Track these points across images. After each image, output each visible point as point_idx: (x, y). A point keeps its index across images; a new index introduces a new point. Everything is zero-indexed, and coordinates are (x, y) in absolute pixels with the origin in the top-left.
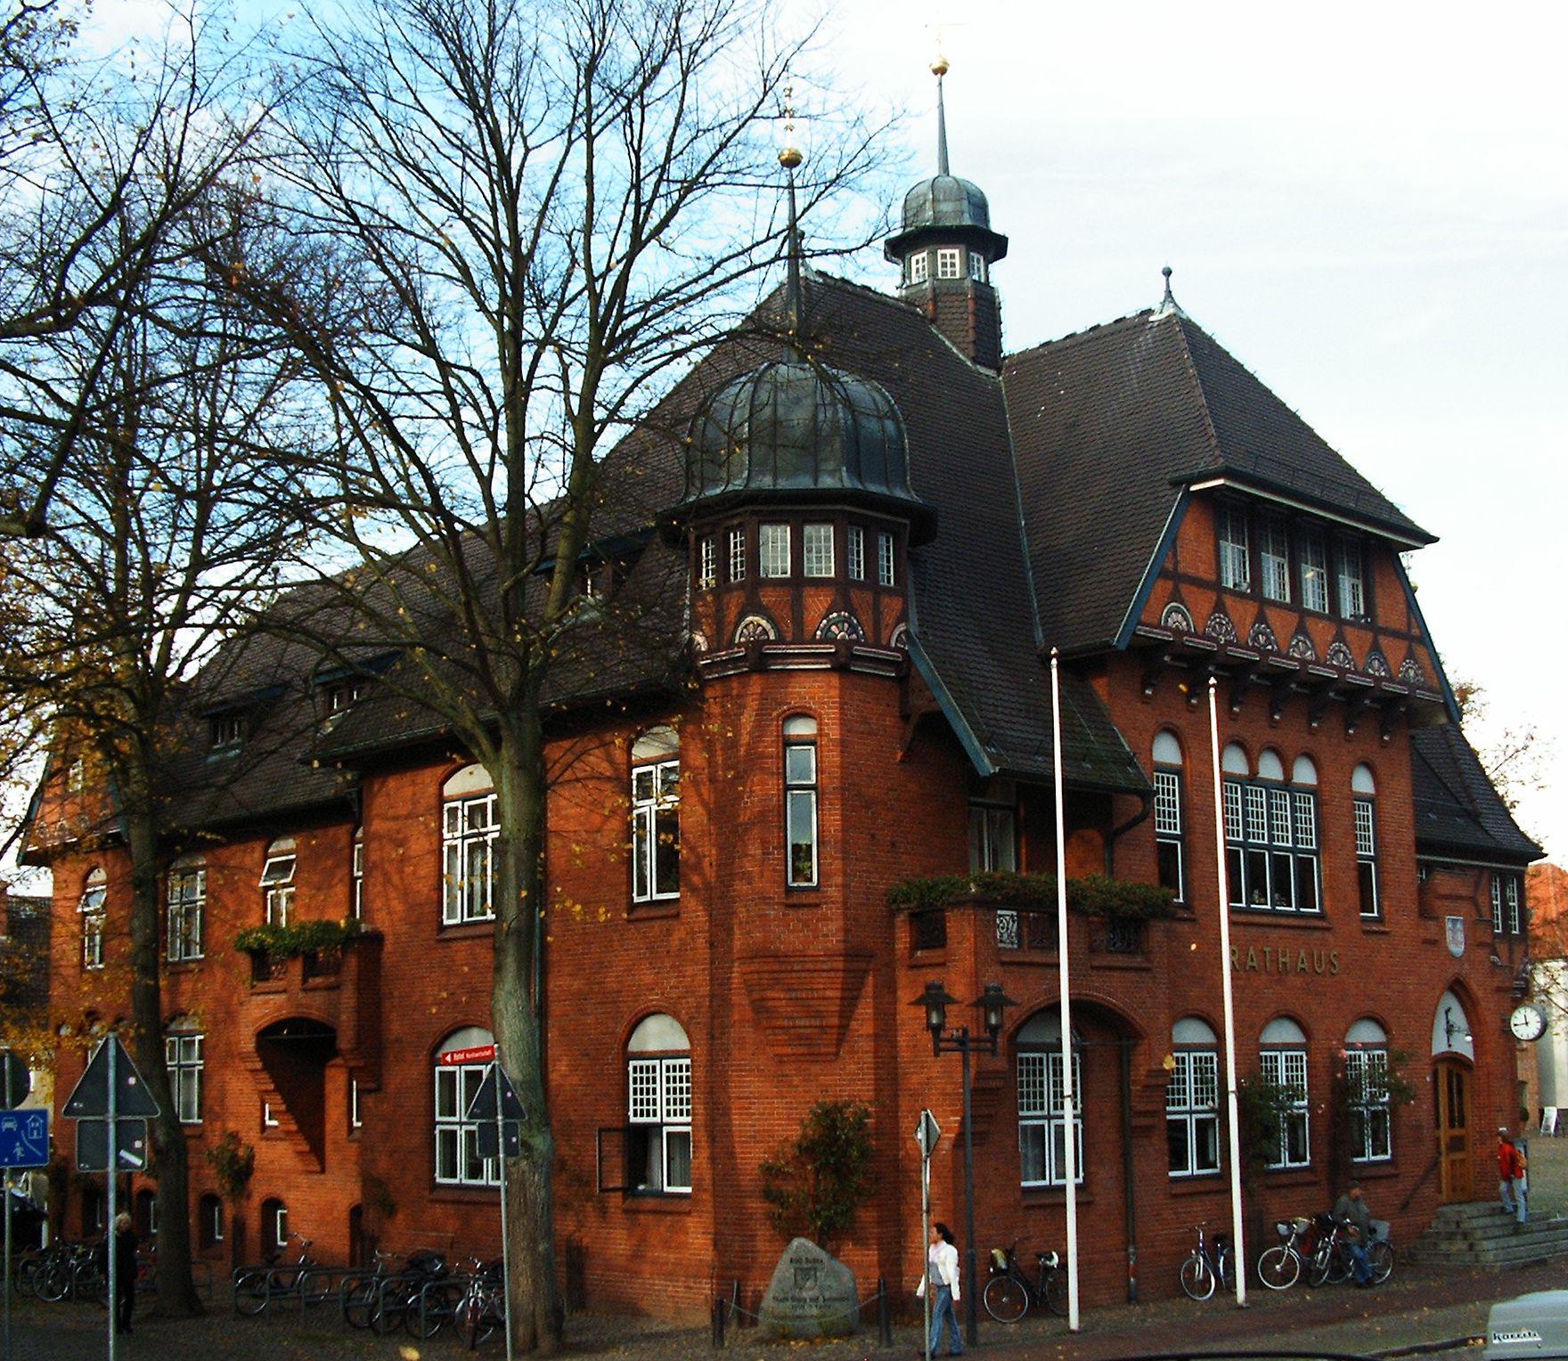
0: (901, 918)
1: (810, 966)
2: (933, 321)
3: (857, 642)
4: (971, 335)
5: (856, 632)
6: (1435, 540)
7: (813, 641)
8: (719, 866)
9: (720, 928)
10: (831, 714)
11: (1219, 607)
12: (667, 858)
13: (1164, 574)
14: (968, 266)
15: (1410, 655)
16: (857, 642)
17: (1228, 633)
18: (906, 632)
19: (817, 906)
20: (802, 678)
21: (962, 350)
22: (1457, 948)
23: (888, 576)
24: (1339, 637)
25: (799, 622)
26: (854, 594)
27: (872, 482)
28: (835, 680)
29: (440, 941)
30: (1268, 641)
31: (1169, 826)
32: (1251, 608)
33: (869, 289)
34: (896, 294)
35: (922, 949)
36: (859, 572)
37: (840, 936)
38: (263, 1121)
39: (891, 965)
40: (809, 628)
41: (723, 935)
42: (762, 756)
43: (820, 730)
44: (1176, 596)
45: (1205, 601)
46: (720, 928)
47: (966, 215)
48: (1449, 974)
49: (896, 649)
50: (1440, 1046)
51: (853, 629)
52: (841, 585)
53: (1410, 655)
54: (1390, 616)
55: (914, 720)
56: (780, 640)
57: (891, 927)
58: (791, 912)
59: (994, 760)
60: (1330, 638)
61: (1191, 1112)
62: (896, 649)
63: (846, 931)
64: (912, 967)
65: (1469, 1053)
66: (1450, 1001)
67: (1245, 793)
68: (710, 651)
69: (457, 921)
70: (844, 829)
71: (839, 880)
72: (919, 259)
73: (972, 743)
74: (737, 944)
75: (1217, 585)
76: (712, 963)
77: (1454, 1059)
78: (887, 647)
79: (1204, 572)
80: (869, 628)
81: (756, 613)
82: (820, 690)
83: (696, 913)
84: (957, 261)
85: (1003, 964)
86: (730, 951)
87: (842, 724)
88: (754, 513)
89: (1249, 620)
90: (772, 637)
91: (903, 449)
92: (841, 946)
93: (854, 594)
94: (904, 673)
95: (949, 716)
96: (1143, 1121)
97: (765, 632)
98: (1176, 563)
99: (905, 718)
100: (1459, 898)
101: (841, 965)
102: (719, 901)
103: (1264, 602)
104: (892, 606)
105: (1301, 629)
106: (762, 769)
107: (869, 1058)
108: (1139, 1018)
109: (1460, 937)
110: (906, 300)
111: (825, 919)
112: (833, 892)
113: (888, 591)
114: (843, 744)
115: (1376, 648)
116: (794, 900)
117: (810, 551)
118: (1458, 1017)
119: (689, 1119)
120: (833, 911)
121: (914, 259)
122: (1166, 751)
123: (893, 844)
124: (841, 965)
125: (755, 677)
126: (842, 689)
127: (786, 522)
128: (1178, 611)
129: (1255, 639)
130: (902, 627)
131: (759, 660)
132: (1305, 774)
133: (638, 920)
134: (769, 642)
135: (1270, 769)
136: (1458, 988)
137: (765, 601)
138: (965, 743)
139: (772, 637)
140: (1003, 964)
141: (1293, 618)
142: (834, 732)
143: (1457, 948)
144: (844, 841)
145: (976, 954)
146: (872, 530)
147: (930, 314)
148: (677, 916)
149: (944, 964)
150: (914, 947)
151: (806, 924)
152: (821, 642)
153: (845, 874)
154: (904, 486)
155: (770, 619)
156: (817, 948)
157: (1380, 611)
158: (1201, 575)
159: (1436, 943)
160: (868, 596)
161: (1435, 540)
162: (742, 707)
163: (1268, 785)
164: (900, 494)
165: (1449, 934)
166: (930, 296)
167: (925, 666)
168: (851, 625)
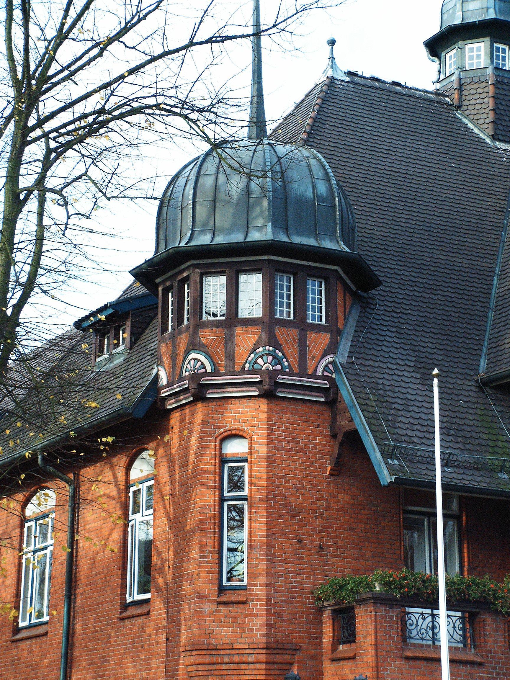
0: (327, 613)
1: (236, 659)
2: (459, 107)
3: (282, 372)
4: (491, 116)
5: (280, 363)
7: (243, 371)
8: (174, 568)
9: (173, 622)
10: (260, 435)
12: (147, 567)
14: (492, 55)
16: (282, 372)
18: (333, 363)
19: (244, 603)
20: (235, 405)
21: (482, 130)
25: (231, 357)
26: (280, 332)
27: (299, 234)
28: (263, 405)
29: (13, 641)
33: (399, 84)
34: (431, 88)
35: (344, 643)
36: (286, 311)
37: (264, 630)
39: (317, 658)
40: (239, 361)
41: (175, 630)
42: (203, 472)
43: (251, 448)
46: (173, 622)
47: (492, 11)
49: (323, 377)
51: (277, 360)
52: (269, 323)
55: (340, 438)
56: (216, 373)
57: (320, 623)
58: (222, 609)
59: (392, 470)
62: (323, 377)
63: (269, 625)
64: (333, 660)
68: (169, 385)
69: (26, 624)
70: (269, 535)
71: (263, 579)
72: (451, 57)
73: (376, 455)
74: (183, 639)
76: (167, 657)
78: (314, 375)
80: (294, 361)
82: (249, 414)
83: (159, 609)
84: (482, 53)
85: (408, 658)
86: (179, 642)
87: (269, 442)
88: (195, 266)
90: (209, 370)
91: (334, 206)
92: (264, 640)
93: (280, 332)
94: (332, 399)
95: (361, 432)
97: (203, 366)
99: (334, 436)
101: (263, 658)
102: (173, 598)
106: (202, 484)
110: (436, 93)
111: (251, 615)
112: (260, 591)
114: (270, 460)
116: (225, 598)
120: (258, 608)
121: (448, 56)
123: (321, 548)
124: (263, 658)
125: (199, 405)
126: (270, 412)
127: (222, 273)
130: (329, 358)
131: (200, 392)
133: (129, 618)
134: (206, 374)
137: (203, 340)
138: (372, 458)
139: (209, 370)
140: (408, 658)
142: (262, 450)
144: (269, 545)
145: (376, 649)
146: (301, 275)
147: (456, 103)
148: (148, 613)
149: (353, 658)
150: (336, 642)
151: (235, 619)
152: (250, 372)
153: (269, 574)
154: (333, 237)
155: (209, 356)
156: (243, 642)
160: (295, 332)
162: (191, 432)
164: (328, 244)
166: (456, 85)
167: (346, 392)
168: (275, 357)
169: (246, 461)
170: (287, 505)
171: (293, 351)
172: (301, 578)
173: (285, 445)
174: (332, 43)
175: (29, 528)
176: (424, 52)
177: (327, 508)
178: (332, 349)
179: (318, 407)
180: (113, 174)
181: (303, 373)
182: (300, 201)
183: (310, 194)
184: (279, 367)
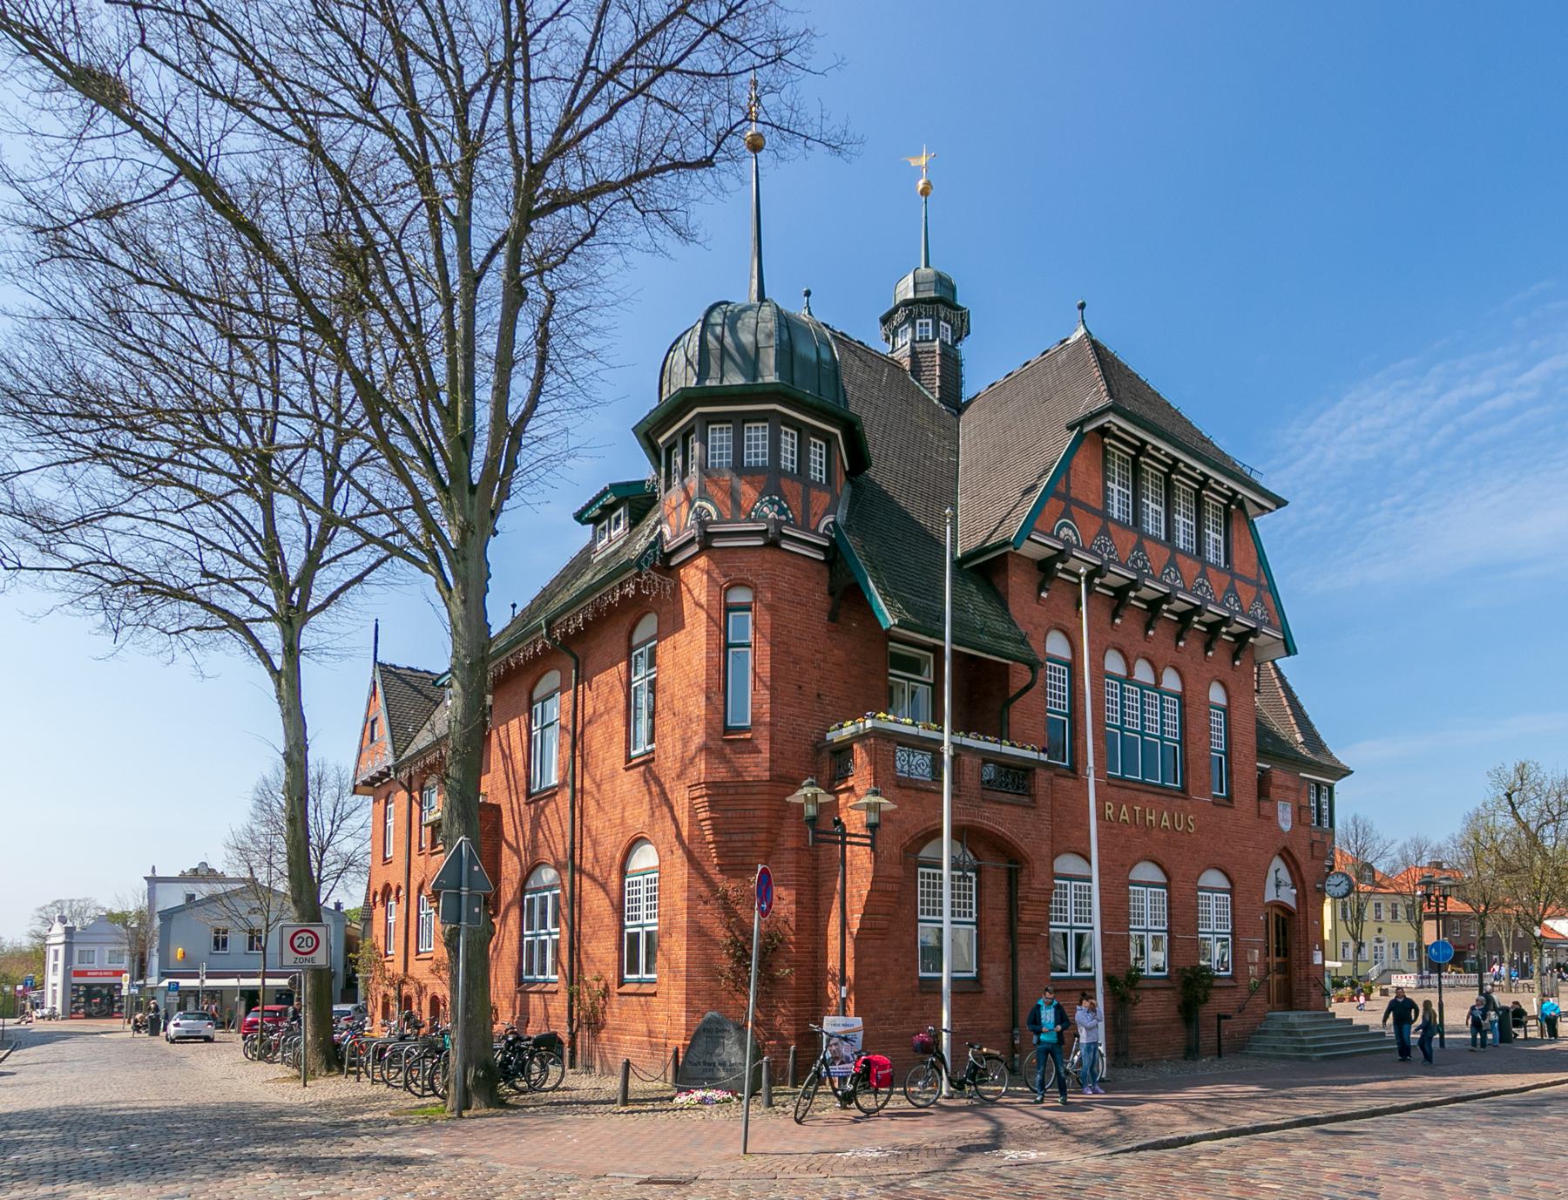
3: (787, 523)
6: (1280, 503)
11: (1104, 531)
13: (1056, 495)
15: (1259, 598)
17: (1111, 553)
18: (834, 523)
22: (1286, 826)
23: (817, 471)
24: (1203, 574)
30: (1145, 566)
31: (1056, 701)
32: (1132, 537)
38: (520, 976)
44: (1066, 513)
45: (1093, 526)
48: (1281, 845)
49: (824, 535)
50: (1270, 895)
51: (782, 511)
53: (1259, 598)
54: (1244, 562)
60: (1195, 573)
61: (1071, 928)
62: (824, 535)
65: (1292, 903)
66: (1277, 863)
67: (1123, 690)
75: (1104, 515)
77: (1282, 906)
78: (815, 532)
79: (1094, 500)
81: (707, 500)
89: (1130, 547)
93: (785, 484)
96: (1029, 930)
98: (1068, 488)
100: (1288, 788)
103: (1144, 535)
104: (821, 499)
105: (1172, 562)
107: (792, 867)
108: (1025, 846)
109: (1289, 817)
113: (817, 485)
115: (1232, 589)
117: (749, 447)
118: (1284, 875)
119: (655, 920)
122: (1056, 645)
128: (1070, 527)
129: (1134, 562)
132: (1171, 681)
135: (1143, 672)
136: (1286, 855)
141: (1166, 552)
143: (1286, 826)
157: (1236, 561)
158: (1092, 504)
159: (1271, 819)
161: (1280, 503)
163: (1142, 686)
165: (1280, 814)
168: (781, 507)
169: (749, 609)
170: (789, 654)
171: (797, 503)
172: (800, 721)
173: (788, 596)
174: (808, 294)
175: (531, 901)
176: (878, 323)
177: (825, 661)
178: (830, 510)
179: (816, 565)
180: (640, 91)
181: (805, 528)
182: (805, 361)
183: (814, 357)
184: (784, 518)
